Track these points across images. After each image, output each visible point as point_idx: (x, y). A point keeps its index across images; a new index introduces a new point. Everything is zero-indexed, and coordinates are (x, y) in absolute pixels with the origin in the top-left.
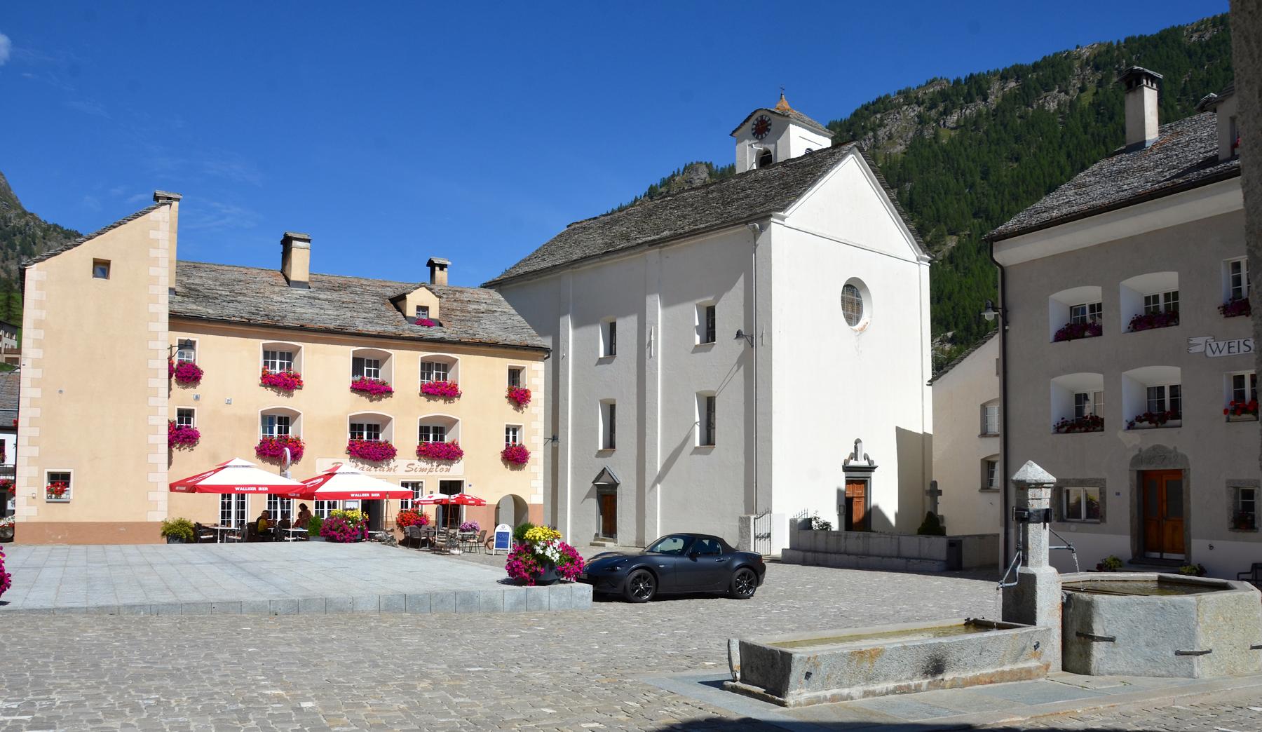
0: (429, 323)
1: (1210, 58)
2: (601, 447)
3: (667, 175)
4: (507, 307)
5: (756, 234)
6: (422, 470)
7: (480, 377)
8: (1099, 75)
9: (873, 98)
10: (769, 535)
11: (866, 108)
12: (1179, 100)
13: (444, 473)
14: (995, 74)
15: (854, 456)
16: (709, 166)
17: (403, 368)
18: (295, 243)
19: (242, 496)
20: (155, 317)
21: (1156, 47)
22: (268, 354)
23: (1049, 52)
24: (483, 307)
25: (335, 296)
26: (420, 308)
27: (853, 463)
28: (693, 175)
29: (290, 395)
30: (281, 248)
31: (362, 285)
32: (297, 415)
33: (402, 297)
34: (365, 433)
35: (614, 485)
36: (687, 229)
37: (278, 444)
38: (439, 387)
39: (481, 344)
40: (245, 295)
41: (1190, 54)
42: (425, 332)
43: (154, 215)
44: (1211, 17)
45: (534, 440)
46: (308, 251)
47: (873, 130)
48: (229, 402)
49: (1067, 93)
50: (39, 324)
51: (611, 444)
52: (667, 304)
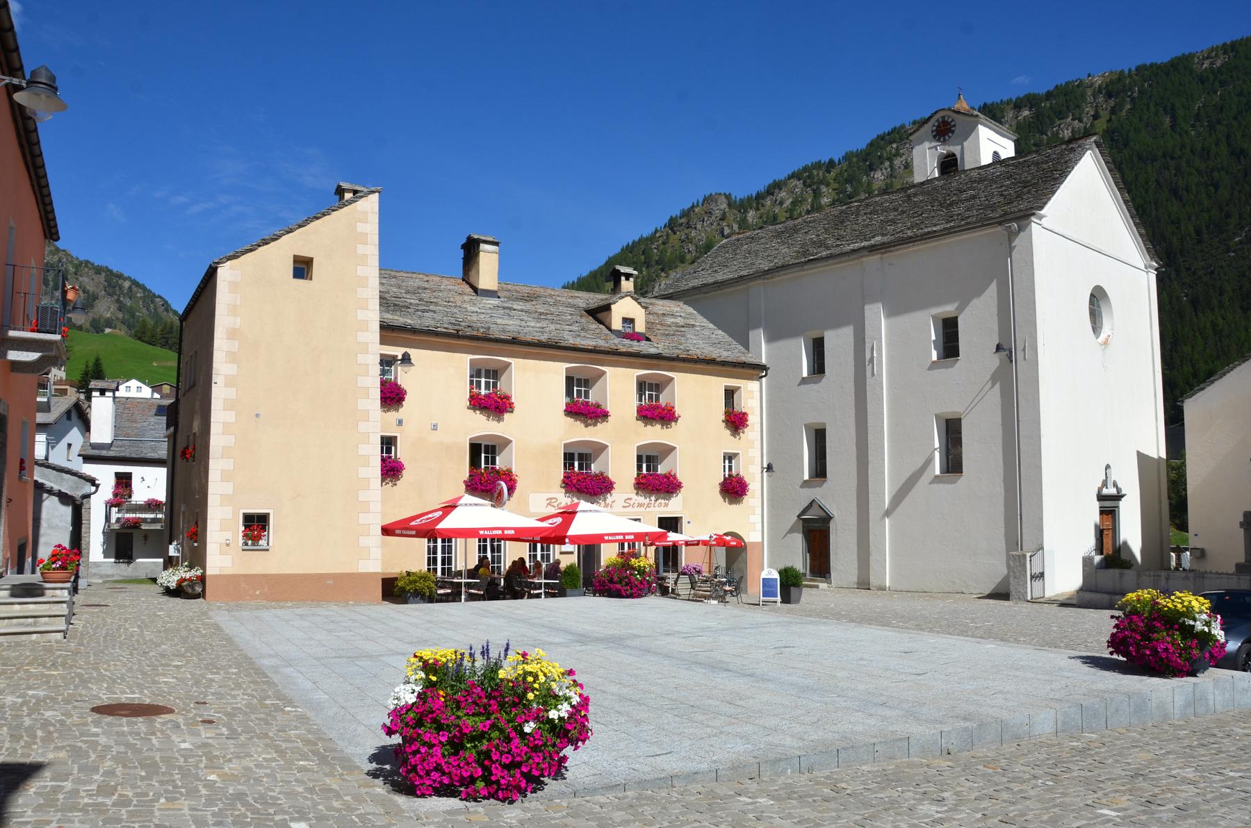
1: (1222, 84)
2: (806, 477)
3: (687, 206)
4: (700, 321)
5: (1012, 235)
6: (640, 505)
7: (695, 395)
8: (1112, 102)
9: (888, 129)
10: (1042, 575)
11: (881, 138)
12: (1193, 126)
13: (662, 509)
14: (1008, 102)
15: (1105, 484)
16: (728, 197)
17: (618, 388)
18: (483, 246)
20: (364, 326)
21: (1167, 74)
22: (476, 373)
23: (1061, 81)
24: (679, 321)
25: (528, 306)
26: (625, 320)
27: (1105, 491)
28: (713, 206)
29: (500, 420)
30: (461, 253)
31: (551, 296)
32: (507, 442)
33: (607, 308)
34: (576, 464)
35: (827, 519)
36: (909, 233)
37: (487, 474)
38: (656, 413)
39: (698, 361)
40: (436, 304)
41: (1202, 81)
42: (636, 346)
44: (1220, 44)
45: (751, 470)
46: (496, 256)
47: (888, 159)
48: (435, 428)
49: (1080, 120)
50: (232, 334)
51: (820, 471)
52: (892, 313)
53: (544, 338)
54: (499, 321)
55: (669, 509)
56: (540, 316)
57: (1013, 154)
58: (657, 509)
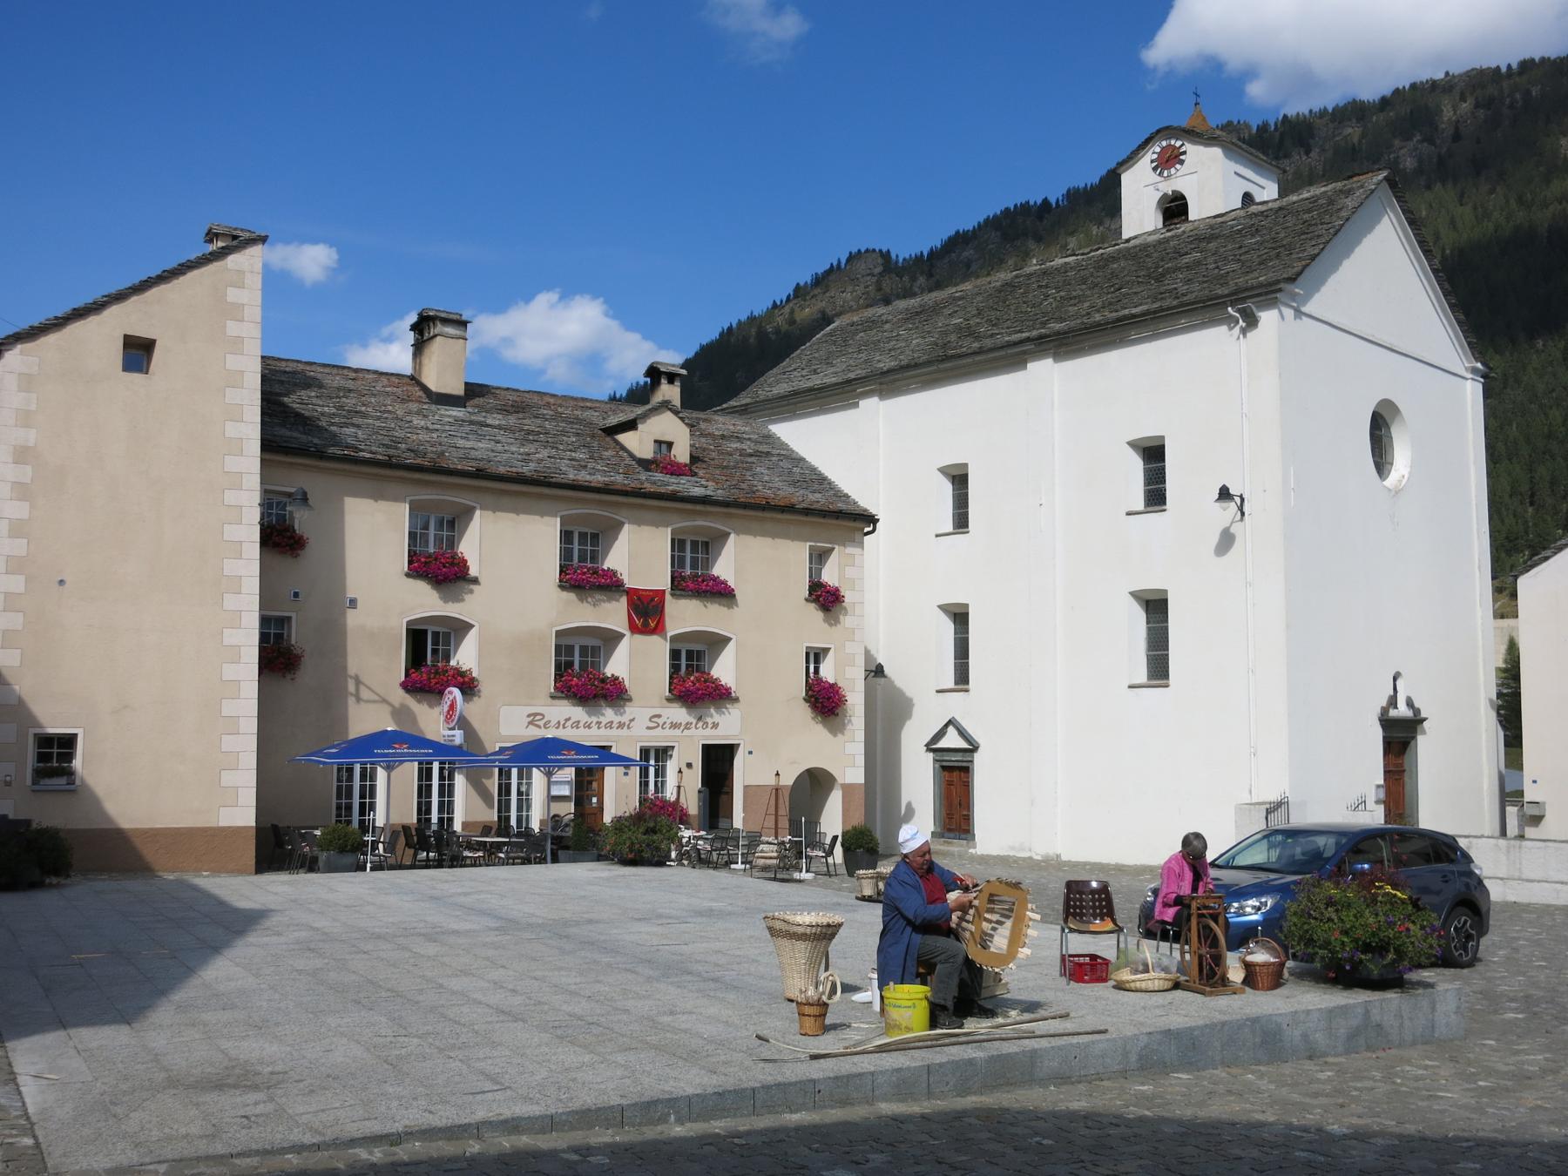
0: (675, 469)
6: (674, 726)
13: (708, 732)
15: (1393, 702)
19: (1503, 833)
24: (748, 447)
25: (512, 420)
36: (1098, 317)
40: (364, 415)
43: (233, 260)
53: (528, 469)
54: (461, 443)
55: (720, 731)
56: (527, 436)
57: (1276, 196)
58: (701, 732)
